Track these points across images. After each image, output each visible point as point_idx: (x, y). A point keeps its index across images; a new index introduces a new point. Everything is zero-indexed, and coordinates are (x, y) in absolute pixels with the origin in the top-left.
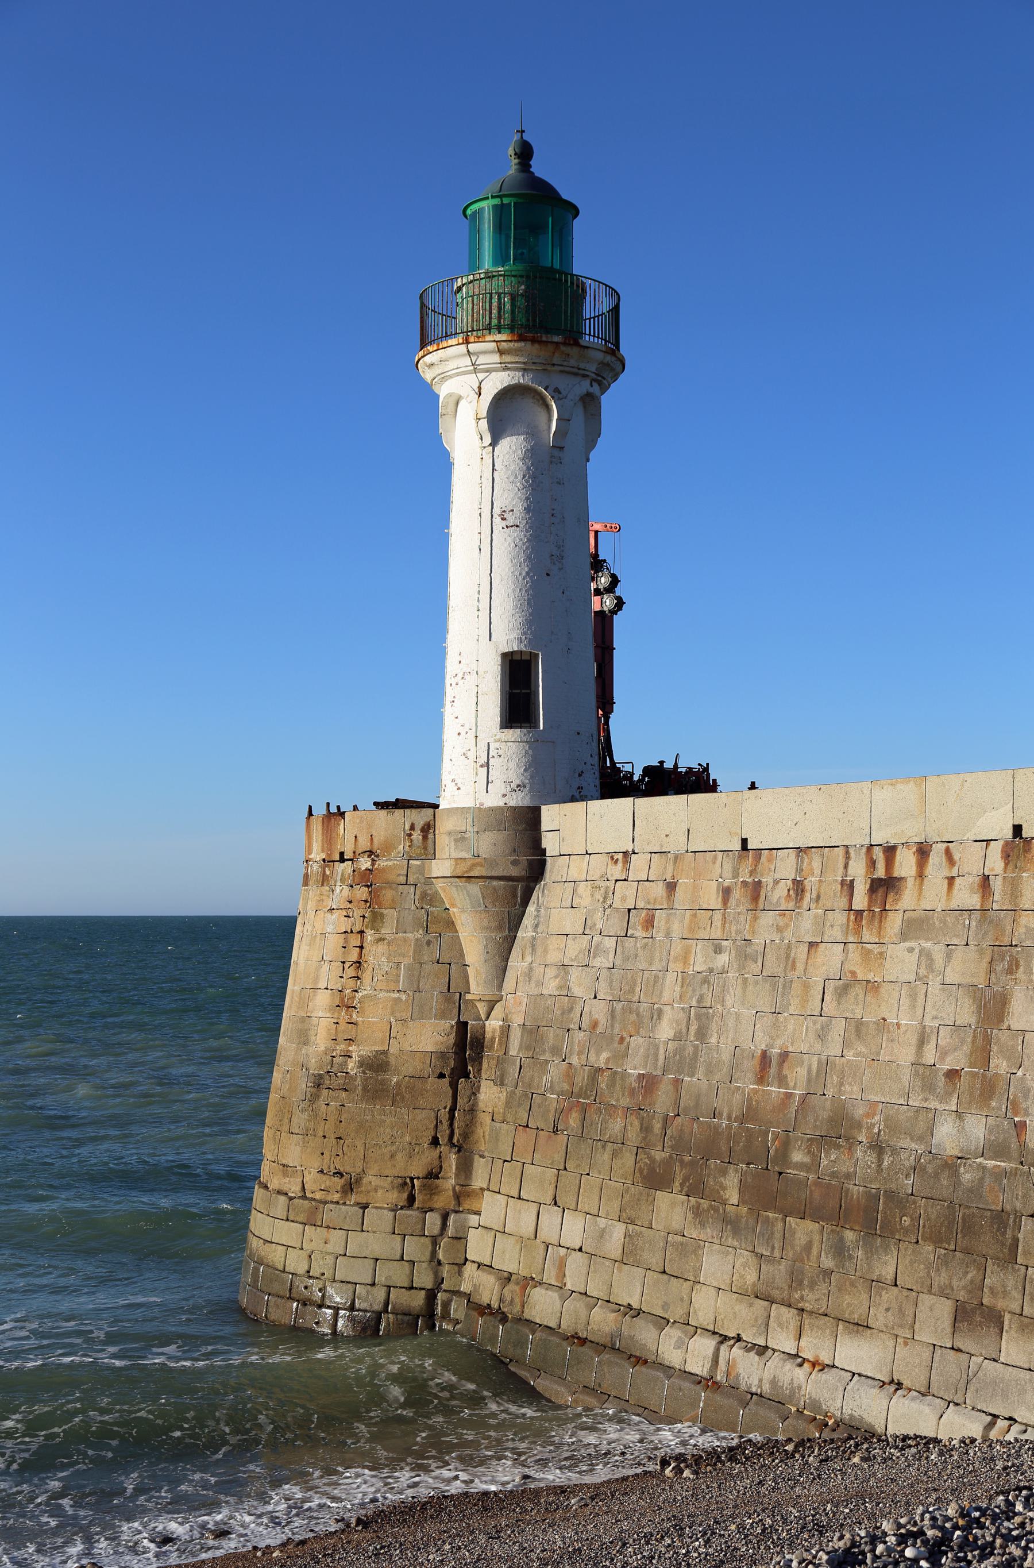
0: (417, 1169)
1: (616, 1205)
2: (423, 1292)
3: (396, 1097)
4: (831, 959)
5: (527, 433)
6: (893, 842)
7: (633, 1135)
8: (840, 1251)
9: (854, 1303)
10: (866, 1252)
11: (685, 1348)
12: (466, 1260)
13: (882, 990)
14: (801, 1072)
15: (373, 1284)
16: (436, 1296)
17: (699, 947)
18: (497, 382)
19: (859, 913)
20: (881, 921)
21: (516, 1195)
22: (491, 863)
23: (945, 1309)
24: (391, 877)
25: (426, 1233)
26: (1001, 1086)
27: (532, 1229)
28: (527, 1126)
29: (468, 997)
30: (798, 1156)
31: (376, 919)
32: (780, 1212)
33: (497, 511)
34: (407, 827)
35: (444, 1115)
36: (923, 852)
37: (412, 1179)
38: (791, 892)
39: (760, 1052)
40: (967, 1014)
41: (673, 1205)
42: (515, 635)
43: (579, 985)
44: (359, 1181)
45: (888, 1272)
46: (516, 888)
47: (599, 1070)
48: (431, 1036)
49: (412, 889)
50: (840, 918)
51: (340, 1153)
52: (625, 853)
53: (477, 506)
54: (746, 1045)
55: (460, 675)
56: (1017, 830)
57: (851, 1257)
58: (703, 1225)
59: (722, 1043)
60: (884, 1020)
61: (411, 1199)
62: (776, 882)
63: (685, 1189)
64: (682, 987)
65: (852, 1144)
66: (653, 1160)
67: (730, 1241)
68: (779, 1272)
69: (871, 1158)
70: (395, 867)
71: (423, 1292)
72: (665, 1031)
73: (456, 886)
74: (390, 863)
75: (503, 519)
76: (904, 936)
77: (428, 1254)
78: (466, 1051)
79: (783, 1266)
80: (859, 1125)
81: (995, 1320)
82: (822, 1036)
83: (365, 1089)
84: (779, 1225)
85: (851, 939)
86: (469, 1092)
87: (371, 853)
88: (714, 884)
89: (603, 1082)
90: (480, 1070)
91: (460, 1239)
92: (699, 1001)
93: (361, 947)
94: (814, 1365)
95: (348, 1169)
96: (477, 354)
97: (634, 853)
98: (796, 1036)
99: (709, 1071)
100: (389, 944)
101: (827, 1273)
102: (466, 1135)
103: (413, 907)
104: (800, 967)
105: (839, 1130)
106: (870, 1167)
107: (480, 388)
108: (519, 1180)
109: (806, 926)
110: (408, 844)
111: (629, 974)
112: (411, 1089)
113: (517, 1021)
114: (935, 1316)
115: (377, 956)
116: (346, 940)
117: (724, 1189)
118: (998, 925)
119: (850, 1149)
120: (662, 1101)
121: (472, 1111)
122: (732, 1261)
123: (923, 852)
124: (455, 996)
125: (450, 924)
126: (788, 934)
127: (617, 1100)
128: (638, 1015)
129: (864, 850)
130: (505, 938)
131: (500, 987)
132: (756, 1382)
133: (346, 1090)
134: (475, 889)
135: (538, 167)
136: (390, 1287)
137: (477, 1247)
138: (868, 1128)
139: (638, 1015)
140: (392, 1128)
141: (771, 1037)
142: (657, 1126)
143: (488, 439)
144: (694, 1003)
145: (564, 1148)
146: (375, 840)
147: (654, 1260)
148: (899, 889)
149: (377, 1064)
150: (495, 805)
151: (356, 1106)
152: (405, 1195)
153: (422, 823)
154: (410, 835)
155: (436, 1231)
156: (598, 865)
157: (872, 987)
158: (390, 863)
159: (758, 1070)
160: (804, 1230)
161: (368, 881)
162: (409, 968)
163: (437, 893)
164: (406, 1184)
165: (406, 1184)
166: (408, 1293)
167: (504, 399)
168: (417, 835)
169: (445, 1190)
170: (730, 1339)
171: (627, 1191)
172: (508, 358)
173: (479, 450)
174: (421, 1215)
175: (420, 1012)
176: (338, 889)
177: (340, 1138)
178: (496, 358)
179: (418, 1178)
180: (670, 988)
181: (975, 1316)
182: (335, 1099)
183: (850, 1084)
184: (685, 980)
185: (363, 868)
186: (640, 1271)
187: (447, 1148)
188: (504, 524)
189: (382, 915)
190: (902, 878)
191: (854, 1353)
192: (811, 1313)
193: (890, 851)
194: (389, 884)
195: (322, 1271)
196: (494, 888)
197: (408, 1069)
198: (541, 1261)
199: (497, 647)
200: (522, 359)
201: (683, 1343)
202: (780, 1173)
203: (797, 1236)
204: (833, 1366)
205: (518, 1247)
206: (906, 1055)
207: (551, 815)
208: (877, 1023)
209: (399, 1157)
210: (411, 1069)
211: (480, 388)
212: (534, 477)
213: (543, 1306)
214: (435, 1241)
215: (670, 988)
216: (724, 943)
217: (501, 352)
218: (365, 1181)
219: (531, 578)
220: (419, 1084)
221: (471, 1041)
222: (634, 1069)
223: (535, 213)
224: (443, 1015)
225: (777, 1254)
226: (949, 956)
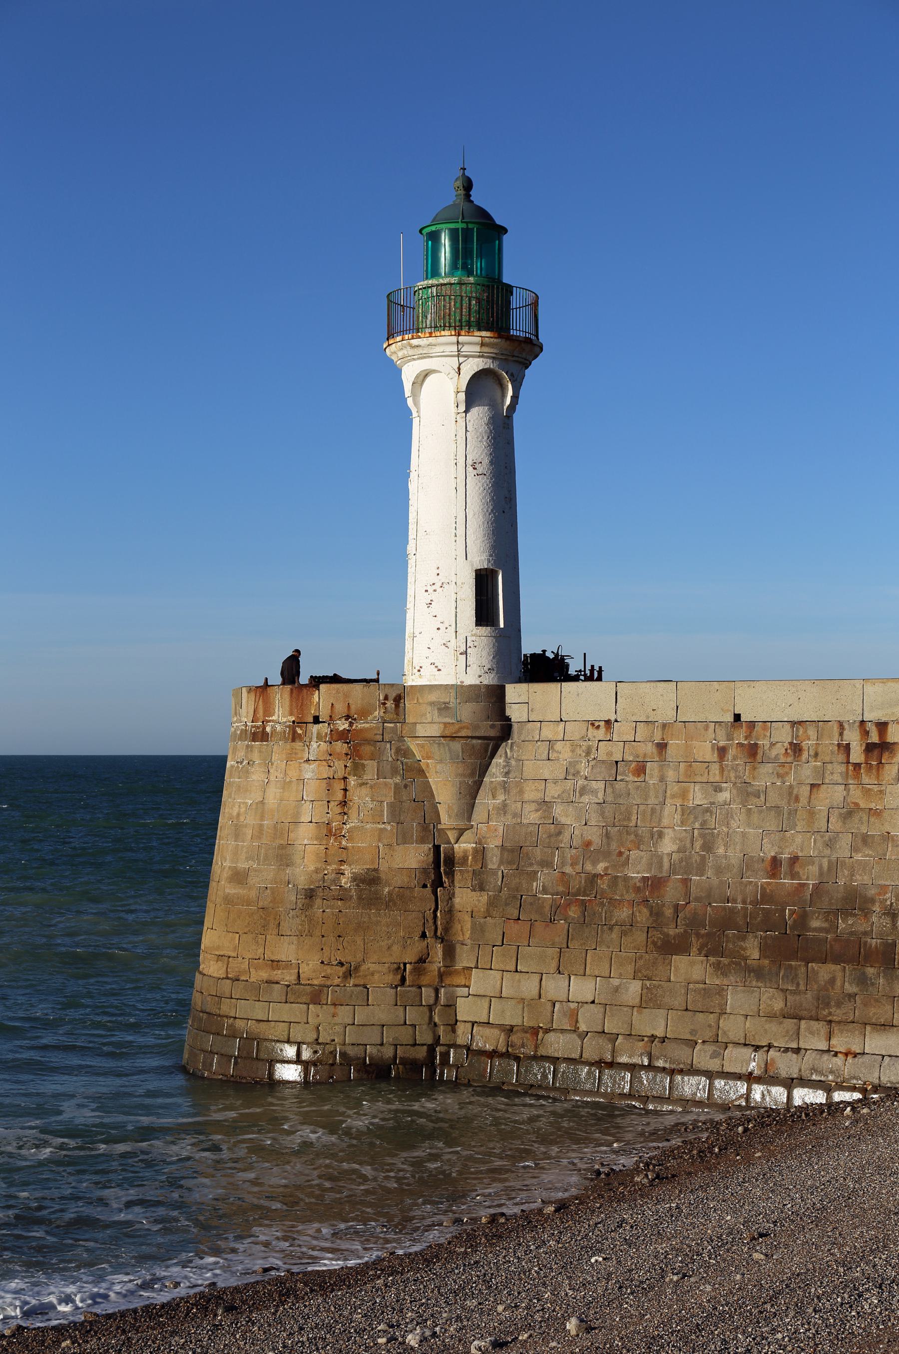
0: (410, 956)
1: (630, 969)
2: (425, 1047)
3: (390, 903)
5: (489, 405)
6: (883, 720)
8: (863, 981)
9: (881, 1012)
10: (887, 980)
11: (721, 1057)
12: (457, 1021)
13: (884, 814)
14: (814, 869)
15: (382, 1044)
16: (435, 1050)
17: (697, 789)
19: (857, 766)
20: (878, 770)
21: (513, 969)
22: (476, 727)
24: (369, 736)
25: (424, 1003)
27: (537, 991)
28: (519, 919)
29: (439, 827)
30: (815, 923)
31: (358, 769)
32: (802, 960)
33: (470, 462)
34: (381, 698)
35: (429, 914)
37: (405, 964)
38: (789, 751)
39: (770, 858)
41: (692, 964)
42: (485, 557)
43: (563, 814)
44: (357, 968)
46: (488, 745)
47: (596, 876)
48: (414, 856)
49: (388, 745)
50: (837, 770)
51: (341, 947)
52: (608, 722)
53: (453, 457)
54: (755, 853)
55: (438, 584)
57: (873, 984)
58: (725, 975)
59: (728, 853)
60: (889, 833)
61: (403, 980)
62: (773, 745)
63: (704, 952)
64: (683, 815)
65: (867, 913)
66: (668, 935)
67: (754, 983)
68: (808, 999)
69: (886, 921)
70: (371, 729)
71: (425, 1047)
72: (668, 846)
73: (439, 744)
74: (368, 725)
75: (475, 469)
77: (427, 1019)
78: (441, 868)
79: (809, 995)
80: (873, 901)
83: (360, 898)
84: (803, 969)
85: (851, 782)
86: (447, 897)
87: (348, 717)
88: (708, 745)
89: (603, 884)
90: (453, 881)
91: (451, 1006)
92: (701, 824)
93: (345, 790)
94: (846, 1054)
95: (349, 959)
96: (463, 344)
97: (616, 721)
99: (719, 871)
100: (371, 787)
101: (852, 996)
102: (447, 929)
103: (390, 759)
104: (803, 801)
105: (856, 902)
106: (885, 926)
107: (459, 369)
108: (515, 959)
109: (807, 771)
110: (383, 711)
111: (623, 808)
112: (401, 897)
113: (493, 844)
115: (360, 797)
116: (329, 784)
117: (744, 949)
119: (865, 916)
120: (671, 894)
121: (450, 912)
122: (758, 996)
124: (429, 827)
126: (791, 779)
127: (622, 895)
128: (636, 835)
129: (857, 724)
130: (475, 782)
131: (469, 819)
132: (797, 1071)
133: (341, 899)
134: (457, 746)
135: (476, 196)
136: (396, 1045)
137: (465, 1010)
138: (881, 902)
139: (636, 835)
140: (388, 926)
141: (780, 847)
142: (669, 912)
143: (462, 408)
144: (697, 825)
145: (565, 932)
146: (353, 707)
147: (678, 1002)
148: (893, 750)
149: (369, 880)
150: (473, 683)
151: (351, 911)
152: (399, 977)
153: (394, 695)
154: (384, 704)
155: (432, 1001)
156: (575, 731)
158: (368, 725)
159: (769, 869)
160: (824, 971)
161: (347, 738)
162: (391, 806)
163: (408, 747)
164: (400, 969)
165: (400, 969)
166: (412, 1048)
167: (478, 378)
168: (390, 704)
169: (430, 971)
170: (763, 1047)
171: (641, 957)
172: (486, 349)
173: (454, 416)
174: (419, 990)
175: (404, 838)
176: (314, 745)
177: (339, 936)
178: (478, 348)
179: (411, 963)
182: (332, 907)
183: (861, 875)
184: (687, 812)
185: (341, 729)
186: (663, 1012)
187: (433, 940)
188: (475, 472)
189: (363, 766)
190: (894, 743)
192: (839, 1022)
194: (368, 742)
195: (332, 1038)
196: (473, 746)
197: (399, 880)
198: (549, 1014)
199: (472, 565)
200: (495, 351)
201: (719, 1054)
202: (799, 936)
203: (821, 974)
204: (864, 1053)
205: (521, 1006)
207: (515, 692)
208: (882, 835)
209: (395, 948)
210: (399, 882)
211: (459, 369)
212: (494, 438)
214: (431, 1008)
215: (670, 815)
216: (725, 785)
217: (482, 345)
218: (363, 968)
219: (494, 514)
220: (408, 892)
221: (445, 861)
222: (635, 874)
223: (480, 235)
224: (422, 841)
225: (802, 987)
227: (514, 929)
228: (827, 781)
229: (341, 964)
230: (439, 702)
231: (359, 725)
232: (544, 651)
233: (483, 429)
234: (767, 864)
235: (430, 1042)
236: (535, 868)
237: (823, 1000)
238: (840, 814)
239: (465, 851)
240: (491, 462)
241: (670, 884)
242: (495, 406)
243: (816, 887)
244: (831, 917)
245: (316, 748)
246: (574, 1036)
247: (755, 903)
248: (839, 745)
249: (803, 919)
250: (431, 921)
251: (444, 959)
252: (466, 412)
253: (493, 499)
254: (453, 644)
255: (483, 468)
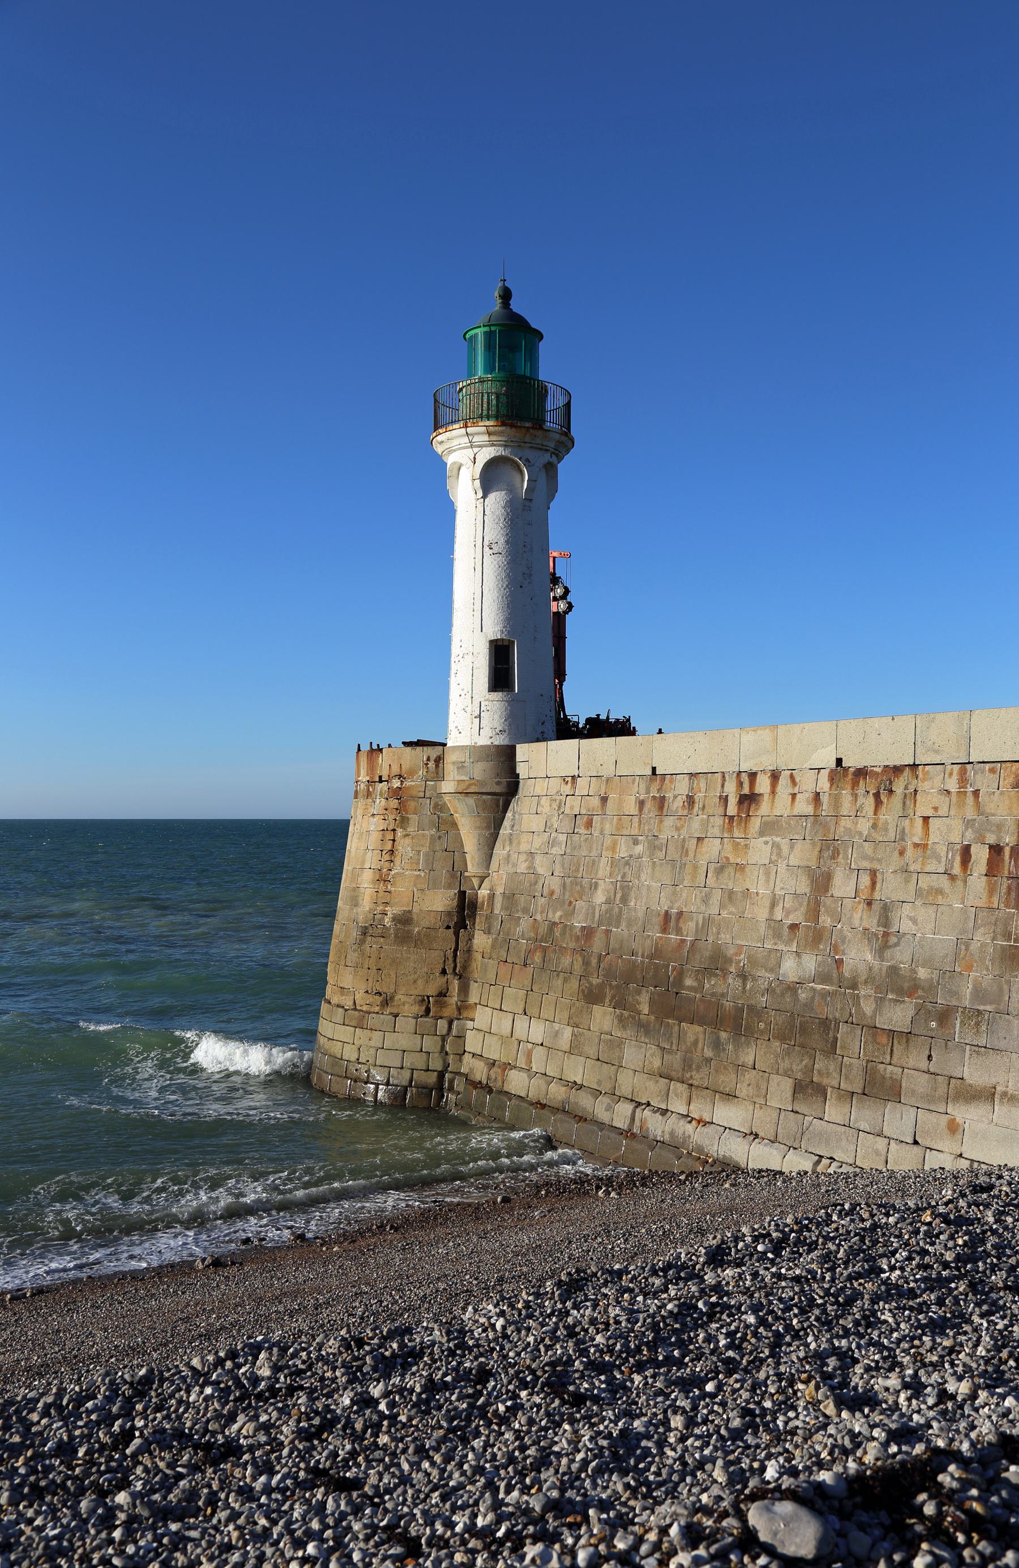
0: (432, 990)
1: (566, 1015)
4: (712, 848)
6: (754, 770)
7: (578, 967)
13: (747, 870)
14: (692, 925)
15: (402, 1068)
18: (486, 454)
19: (731, 818)
23: (788, 1084)
24: (414, 793)
26: (827, 934)
29: (466, 874)
30: (689, 982)
31: (404, 822)
32: (677, 1019)
33: (486, 543)
35: (450, 954)
36: (775, 776)
37: (428, 997)
40: (804, 886)
42: (498, 628)
44: (392, 998)
45: (749, 1060)
46: (498, 801)
47: (555, 924)
48: (440, 901)
50: (718, 821)
52: (573, 777)
53: (473, 539)
56: (839, 761)
59: (637, 906)
61: (428, 1011)
62: (675, 797)
65: (725, 973)
66: (591, 984)
68: (676, 1060)
69: (738, 983)
76: (762, 834)
78: (465, 911)
79: (679, 1056)
81: (822, 1092)
82: (706, 900)
83: (396, 936)
84: (676, 1028)
85: (726, 835)
87: (400, 776)
90: (474, 924)
91: (461, 1037)
92: (623, 877)
93: (394, 840)
94: (699, 1122)
95: (385, 990)
96: (473, 435)
98: (689, 901)
99: (629, 925)
101: (708, 1061)
102: (465, 968)
104: (691, 854)
105: (717, 964)
112: (427, 936)
113: (499, 890)
114: (781, 1089)
115: (404, 847)
117: (639, 1003)
118: (825, 826)
120: (597, 945)
121: (469, 951)
123: (775, 776)
124: (457, 873)
125: (454, 825)
126: (684, 833)
130: (491, 834)
131: (488, 867)
135: (515, 306)
137: (472, 1042)
142: (594, 961)
143: (480, 494)
144: (619, 879)
147: (592, 1052)
149: (404, 920)
151: (390, 948)
152: (424, 1008)
155: (444, 1032)
156: (555, 785)
157: (740, 868)
160: (693, 1031)
162: (426, 855)
163: (445, 803)
164: (424, 1000)
165: (424, 1000)
168: (432, 765)
172: (494, 438)
175: (433, 884)
178: (486, 438)
180: (604, 869)
181: (808, 1089)
182: (376, 943)
184: (613, 863)
188: (491, 552)
189: (408, 819)
191: (726, 1114)
192: (697, 1087)
193: (753, 776)
194: (413, 798)
196: (484, 801)
199: (486, 637)
200: (503, 439)
206: (762, 914)
209: (419, 982)
212: (511, 520)
213: (517, 1083)
214: (443, 1039)
215: (604, 869)
218: (397, 998)
220: (433, 933)
223: (513, 338)
224: (449, 886)
225: (674, 1048)
226: (792, 847)
227: (505, 969)
228: (709, 835)
229: (379, 994)
230: (458, 762)
231: (408, 783)
232: (598, 715)
233: (500, 511)
234: (661, 918)
235: (440, 1069)
236: (520, 914)
237: (687, 1064)
238: (716, 869)
239: (484, 897)
240: (507, 542)
241: (598, 934)
242: (511, 490)
243: (693, 943)
244: (700, 977)
245: (380, 802)
246: (525, 1075)
247: (651, 957)
248: (720, 797)
249: (681, 975)
250: (451, 959)
251: (458, 995)
252: (484, 497)
253: (508, 575)
254: (469, 710)
255: (500, 546)
